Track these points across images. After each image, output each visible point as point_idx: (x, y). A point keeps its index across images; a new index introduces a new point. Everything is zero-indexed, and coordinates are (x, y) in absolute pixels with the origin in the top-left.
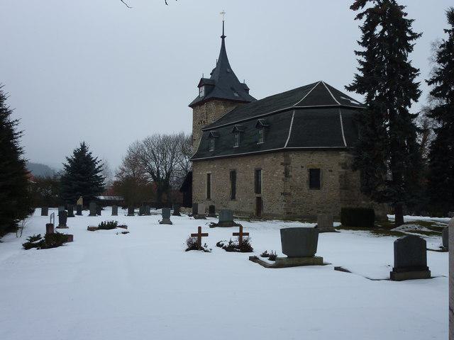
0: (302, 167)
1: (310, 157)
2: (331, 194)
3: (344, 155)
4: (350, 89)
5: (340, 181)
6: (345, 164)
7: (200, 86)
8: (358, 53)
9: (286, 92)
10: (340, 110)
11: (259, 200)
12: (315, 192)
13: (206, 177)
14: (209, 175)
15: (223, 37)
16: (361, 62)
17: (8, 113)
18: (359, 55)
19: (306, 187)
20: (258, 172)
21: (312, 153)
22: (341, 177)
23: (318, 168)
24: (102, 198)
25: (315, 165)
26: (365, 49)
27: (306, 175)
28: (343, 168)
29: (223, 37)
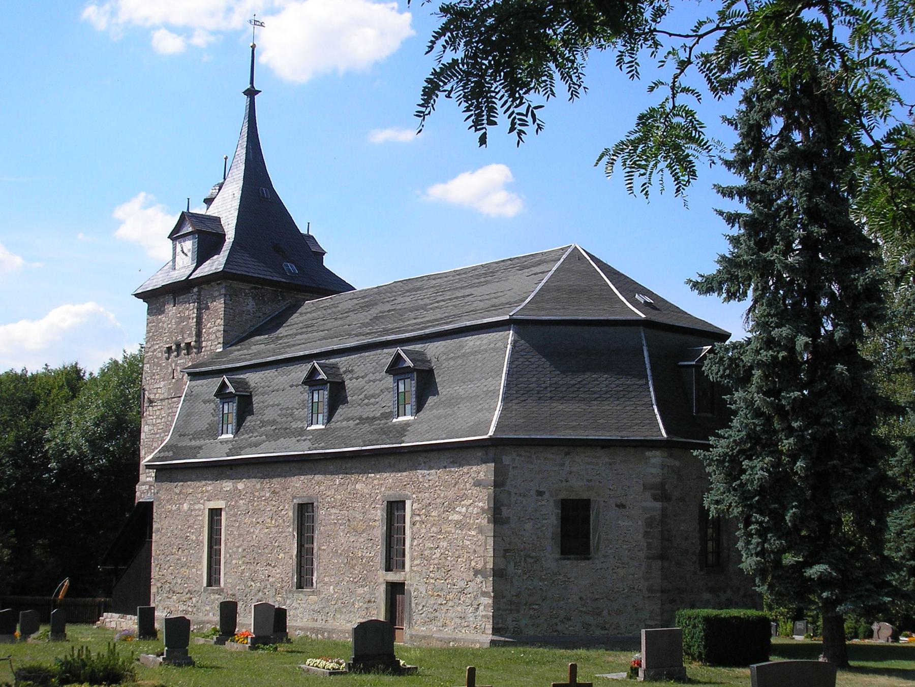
0: (540, 493)
1: (562, 465)
2: (622, 572)
3: (480, 454)
4: (706, 286)
5: (646, 534)
6: (662, 486)
7: (176, 236)
8: (727, 192)
9: (465, 271)
10: (641, 329)
11: (395, 590)
12: (575, 568)
13: (379, 514)
14: (215, 514)
15: (251, 93)
16: (732, 219)
17: (116, 362)
18: (731, 196)
19: (550, 553)
20: (395, 508)
21: (567, 454)
22: (649, 523)
23: (585, 496)
24: (757, 498)
25: (578, 488)
26: (740, 181)
27: (551, 518)
28: (655, 498)
29: (251, 93)
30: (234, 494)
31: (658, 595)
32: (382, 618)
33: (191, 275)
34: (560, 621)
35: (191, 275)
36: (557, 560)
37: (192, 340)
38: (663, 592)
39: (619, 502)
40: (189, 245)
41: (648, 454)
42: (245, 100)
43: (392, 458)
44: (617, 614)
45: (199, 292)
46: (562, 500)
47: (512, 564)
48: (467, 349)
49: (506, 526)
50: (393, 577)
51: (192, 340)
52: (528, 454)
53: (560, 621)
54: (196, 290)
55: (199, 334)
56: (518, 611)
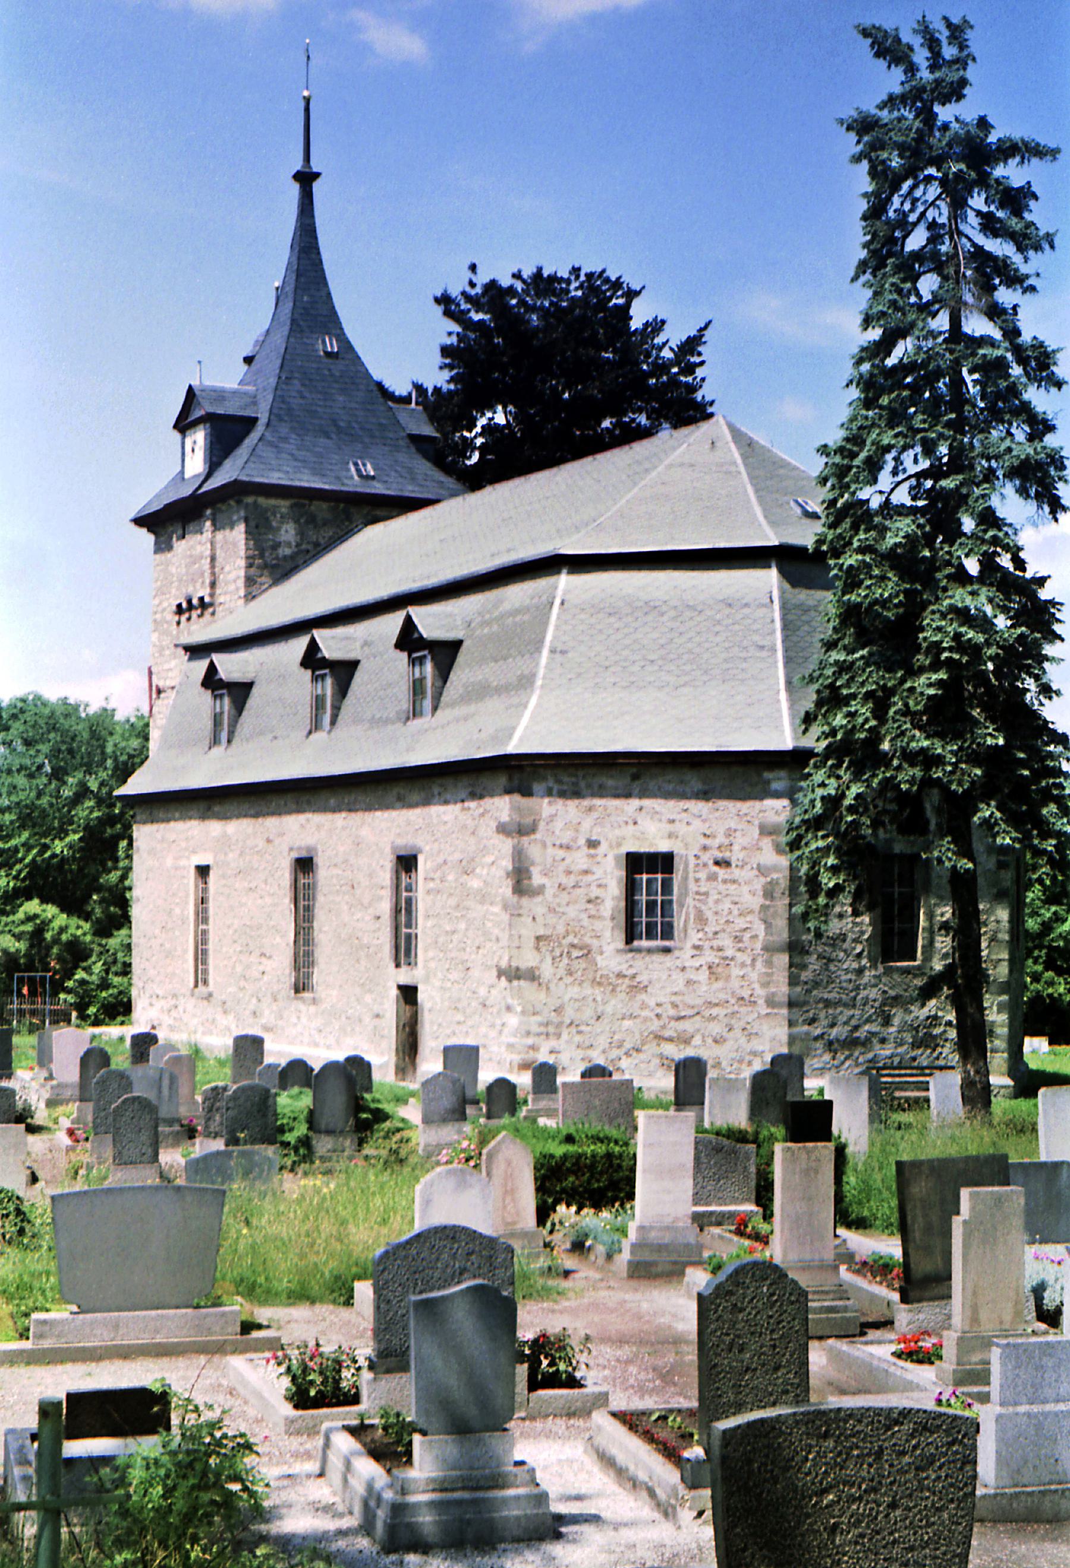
15: (306, 179)
29: (306, 179)
30: (225, 842)
31: (785, 1011)
32: (1027, 1040)
33: (200, 486)
34: (626, 1054)
35: (200, 486)
36: (618, 951)
37: (205, 592)
38: (791, 1004)
39: (719, 855)
40: (199, 437)
41: (767, 775)
42: (295, 189)
43: (580, 773)
44: (716, 1041)
45: (214, 514)
46: (628, 855)
47: (549, 960)
48: (506, 606)
49: (539, 899)
50: (404, 976)
51: (205, 592)
52: (574, 779)
53: (626, 1054)
54: (208, 512)
55: (213, 585)
56: (558, 1036)
